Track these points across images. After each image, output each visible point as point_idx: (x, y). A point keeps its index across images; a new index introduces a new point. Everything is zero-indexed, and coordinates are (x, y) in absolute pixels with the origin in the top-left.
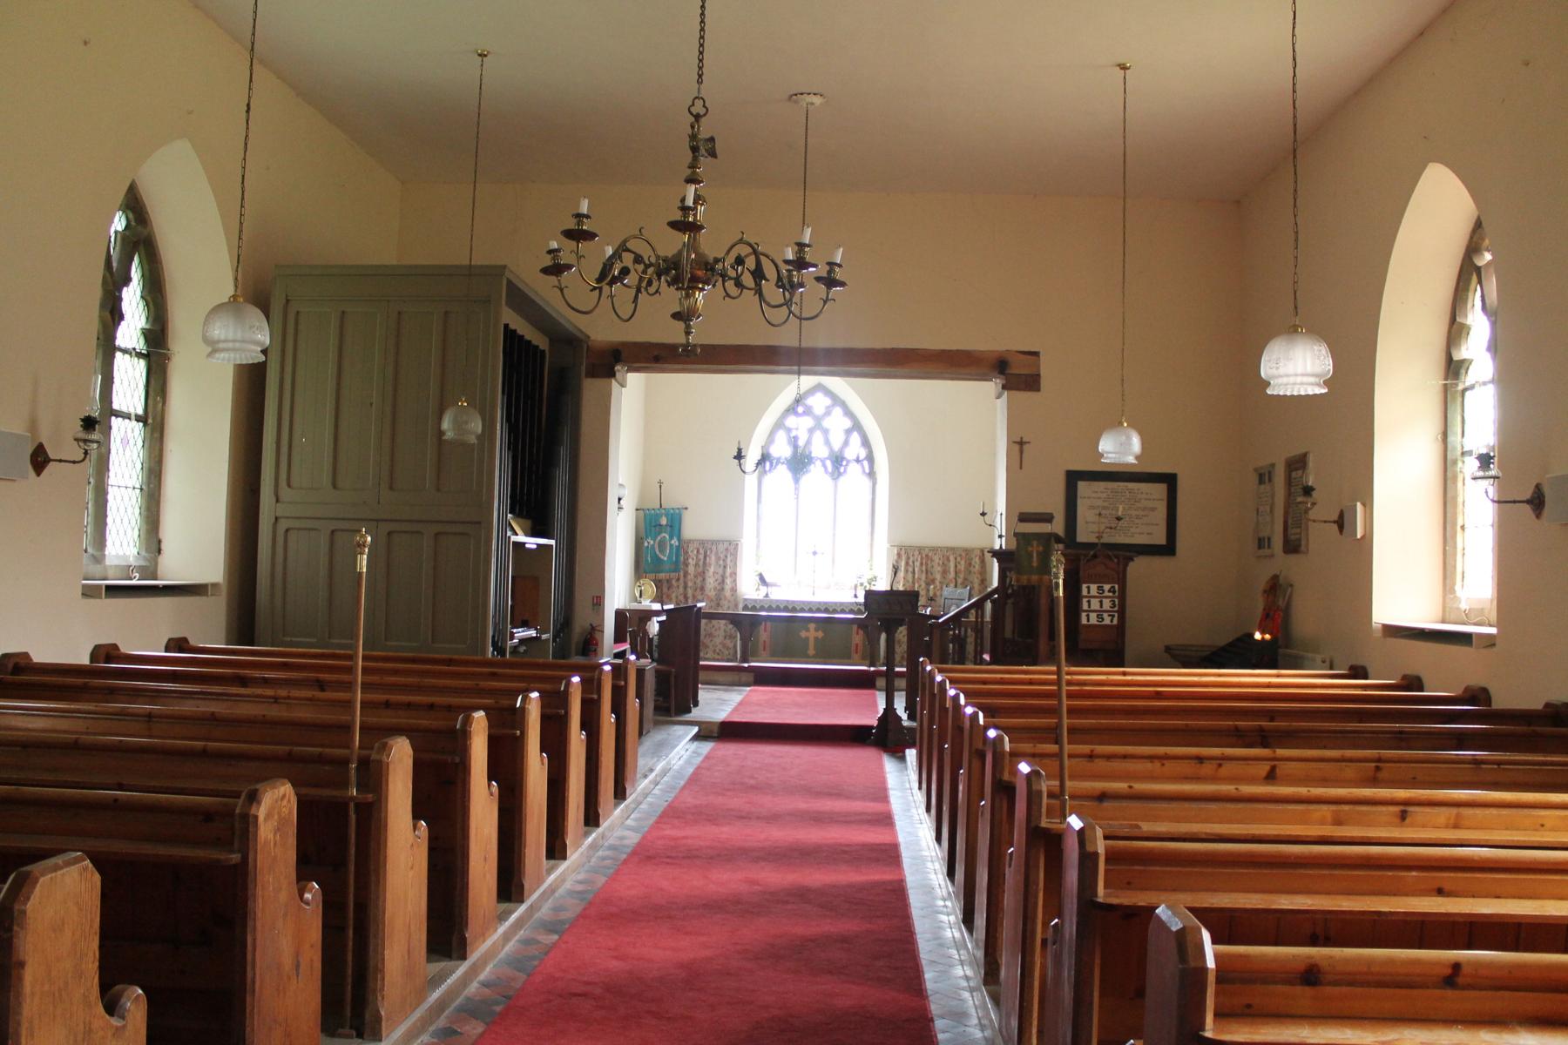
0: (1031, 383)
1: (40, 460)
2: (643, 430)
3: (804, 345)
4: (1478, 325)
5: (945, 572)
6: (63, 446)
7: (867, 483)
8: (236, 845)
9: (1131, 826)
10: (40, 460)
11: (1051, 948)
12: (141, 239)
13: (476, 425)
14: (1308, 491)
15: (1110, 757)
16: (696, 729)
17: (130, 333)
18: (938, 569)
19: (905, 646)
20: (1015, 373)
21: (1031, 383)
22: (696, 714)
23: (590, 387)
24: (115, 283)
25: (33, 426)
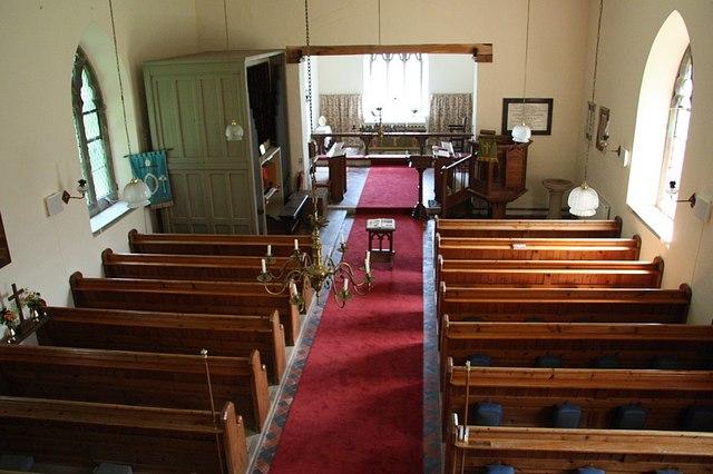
0: (488, 58)
1: (66, 197)
2: (313, 81)
3: (382, 44)
4: (688, 76)
5: (454, 105)
6: (74, 191)
7: (419, 63)
8: (181, 421)
9: (485, 443)
10: (66, 197)
11: (481, 375)
12: (82, 62)
13: (240, 132)
14: (606, 138)
15: (490, 372)
16: (345, 212)
17: (88, 105)
18: (451, 104)
19: (425, 246)
20: (482, 54)
21: (488, 58)
22: (344, 204)
23: (289, 68)
24: (77, 86)
25: (61, 186)
